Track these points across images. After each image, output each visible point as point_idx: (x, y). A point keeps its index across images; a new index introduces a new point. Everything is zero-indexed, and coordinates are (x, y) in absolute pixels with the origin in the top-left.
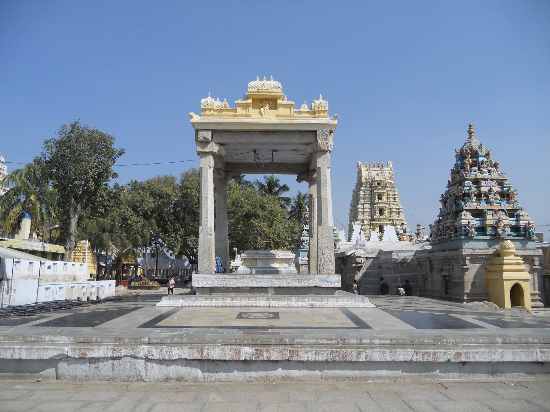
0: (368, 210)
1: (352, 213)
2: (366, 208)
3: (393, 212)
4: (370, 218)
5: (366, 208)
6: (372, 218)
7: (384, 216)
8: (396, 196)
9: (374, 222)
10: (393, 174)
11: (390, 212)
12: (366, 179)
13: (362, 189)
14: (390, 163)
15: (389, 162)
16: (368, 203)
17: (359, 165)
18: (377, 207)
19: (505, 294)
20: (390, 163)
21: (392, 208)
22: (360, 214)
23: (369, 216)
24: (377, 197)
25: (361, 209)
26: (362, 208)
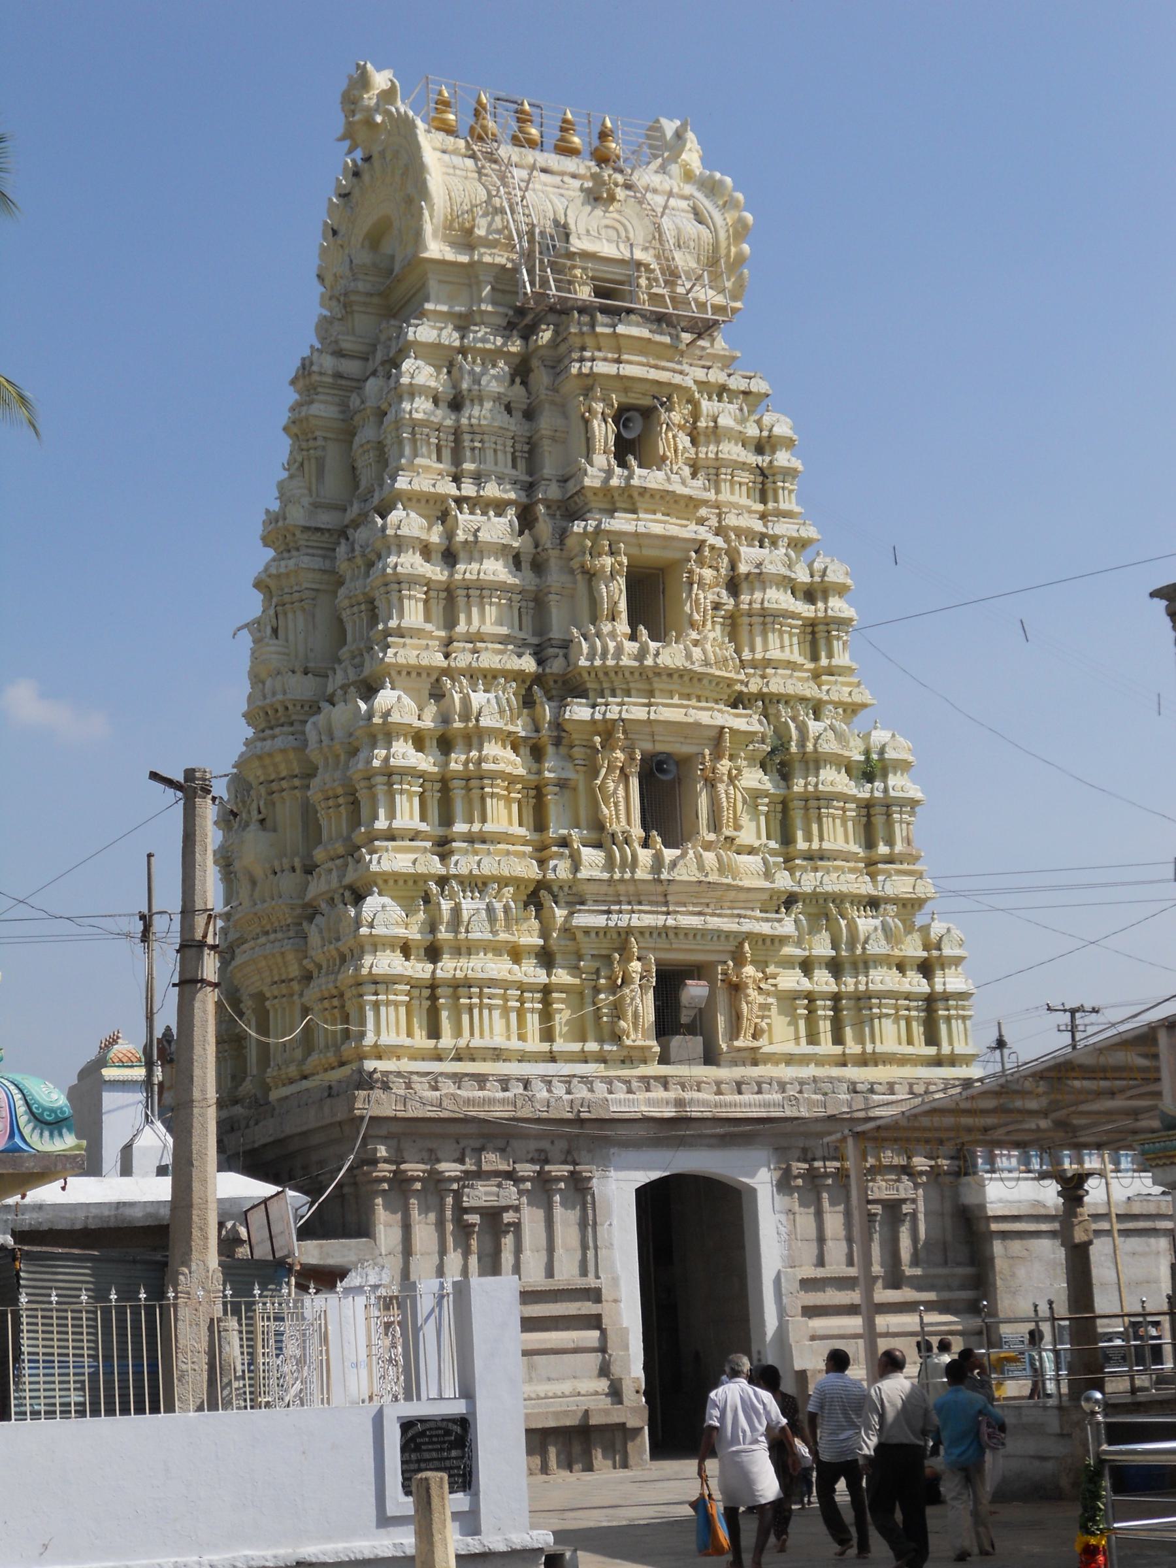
0: (496, 570)
1: (296, 623)
2: (476, 549)
3: (768, 618)
4: (528, 664)
5: (476, 549)
6: (556, 666)
7: (697, 652)
8: (783, 458)
9: (579, 711)
10: (740, 232)
11: (444, 783)
12: (465, 239)
13: (423, 332)
14: (679, 135)
15: (670, 127)
16: (492, 490)
17: (370, 98)
18: (615, 538)
19: (762, 1233)
20: (679, 135)
21: (759, 579)
22: (413, 614)
23: (521, 647)
24: (603, 432)
25: (417, 559)
26: (426, 551)
